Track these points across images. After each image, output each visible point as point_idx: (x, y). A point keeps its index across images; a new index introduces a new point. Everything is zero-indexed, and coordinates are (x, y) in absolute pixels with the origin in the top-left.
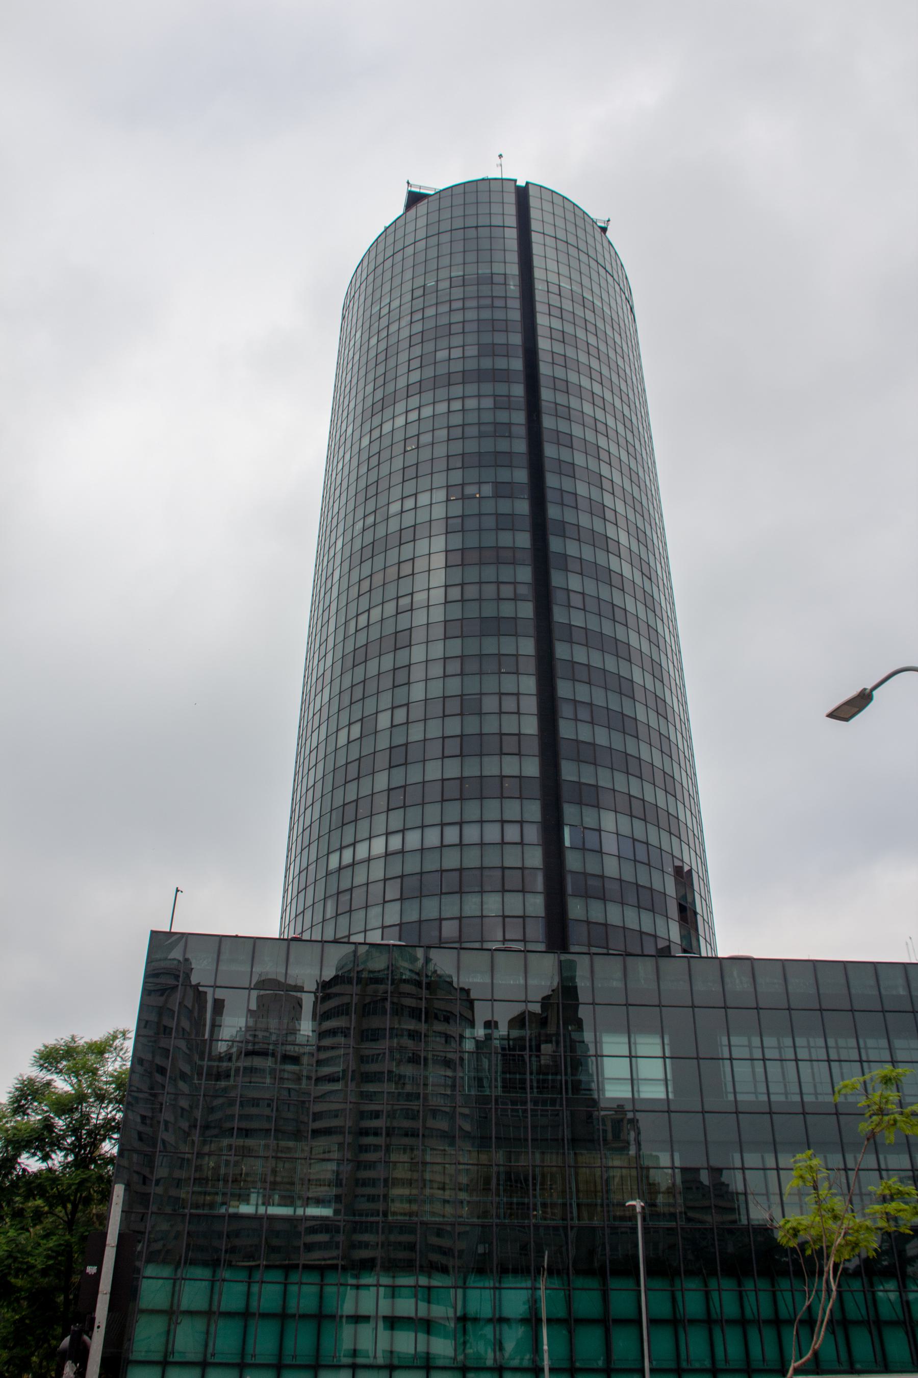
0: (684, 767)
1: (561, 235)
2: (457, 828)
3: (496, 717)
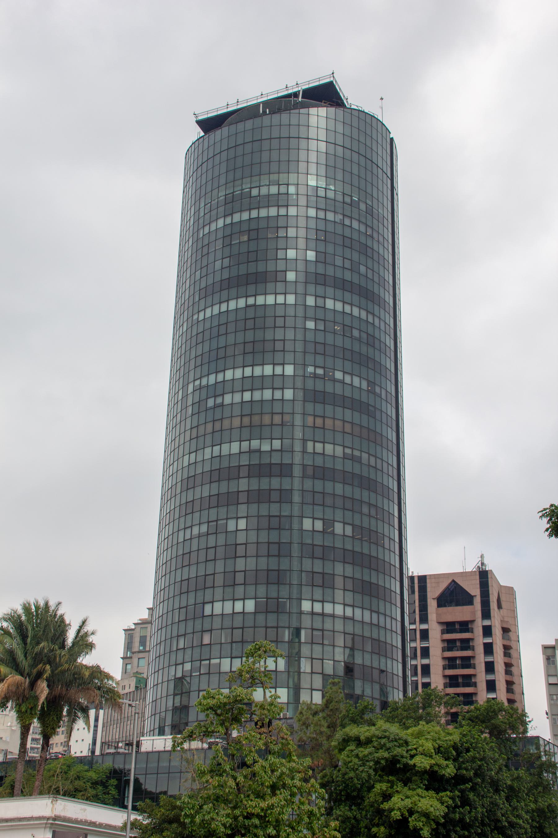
0: (385, 148)
1: (355, 148)
2: (249, 417)
3: (272, 330)
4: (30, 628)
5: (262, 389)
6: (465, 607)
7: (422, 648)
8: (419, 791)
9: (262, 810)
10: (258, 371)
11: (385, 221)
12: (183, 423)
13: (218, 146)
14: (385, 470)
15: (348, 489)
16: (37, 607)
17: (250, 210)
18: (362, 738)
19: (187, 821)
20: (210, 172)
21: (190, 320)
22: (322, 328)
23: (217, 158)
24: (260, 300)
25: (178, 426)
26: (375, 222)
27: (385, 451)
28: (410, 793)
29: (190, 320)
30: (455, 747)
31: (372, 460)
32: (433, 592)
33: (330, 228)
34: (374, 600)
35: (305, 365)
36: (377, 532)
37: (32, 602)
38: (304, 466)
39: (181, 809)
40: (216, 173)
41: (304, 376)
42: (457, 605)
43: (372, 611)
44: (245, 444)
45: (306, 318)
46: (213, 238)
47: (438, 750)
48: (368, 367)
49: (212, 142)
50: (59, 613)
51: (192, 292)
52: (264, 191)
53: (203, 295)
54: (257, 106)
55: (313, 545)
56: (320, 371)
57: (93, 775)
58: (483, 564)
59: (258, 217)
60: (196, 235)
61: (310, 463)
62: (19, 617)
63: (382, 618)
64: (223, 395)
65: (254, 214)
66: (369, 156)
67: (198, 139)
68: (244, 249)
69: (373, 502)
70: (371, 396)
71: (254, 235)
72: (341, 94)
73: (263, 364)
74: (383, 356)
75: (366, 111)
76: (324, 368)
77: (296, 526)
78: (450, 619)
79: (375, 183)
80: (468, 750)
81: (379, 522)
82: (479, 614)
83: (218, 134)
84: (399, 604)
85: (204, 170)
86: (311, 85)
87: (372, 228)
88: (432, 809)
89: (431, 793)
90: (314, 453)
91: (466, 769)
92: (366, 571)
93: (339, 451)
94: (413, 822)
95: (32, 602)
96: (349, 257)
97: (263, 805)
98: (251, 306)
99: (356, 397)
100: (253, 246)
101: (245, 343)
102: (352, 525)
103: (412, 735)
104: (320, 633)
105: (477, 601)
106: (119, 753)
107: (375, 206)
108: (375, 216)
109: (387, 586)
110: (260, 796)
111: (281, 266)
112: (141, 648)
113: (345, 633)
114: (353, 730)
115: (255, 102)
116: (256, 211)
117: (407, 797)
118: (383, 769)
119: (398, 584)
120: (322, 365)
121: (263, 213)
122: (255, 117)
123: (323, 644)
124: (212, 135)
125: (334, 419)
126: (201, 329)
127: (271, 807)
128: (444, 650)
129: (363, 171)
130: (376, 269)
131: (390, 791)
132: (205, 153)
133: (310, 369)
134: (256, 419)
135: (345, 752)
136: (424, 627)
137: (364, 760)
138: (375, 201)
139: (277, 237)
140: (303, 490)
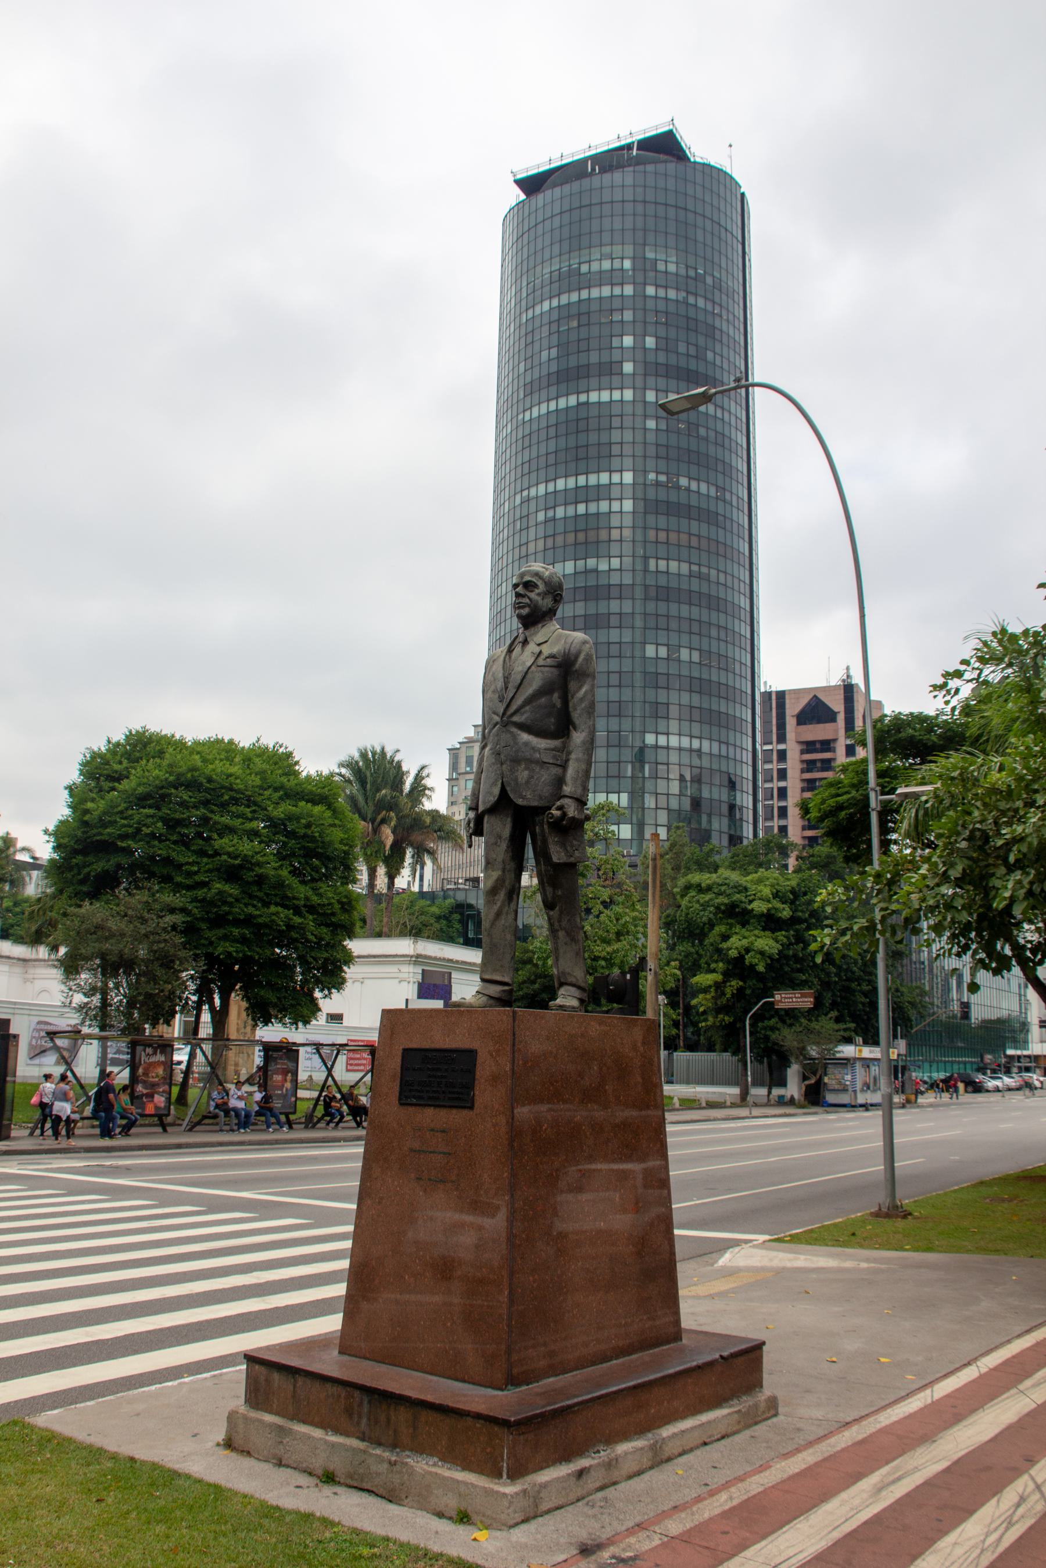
4: (368, 774)
5: (598, 500)
6: (828, 725)
7: (778, 770)
8: (756, 932)
9: (608, 953)
10: (593, 479)
11: (736, 296)
12: (511, 539)
13: (540, 212)
14: (736, 587)
15: (695, 610)
16: (374, 753)
17: (579, 289)
18: (703, 885)
19: (540, 963)
20: (532, 244)
21: (514, 421)
22: (664, 428)
23: (540, 227)
24: (594, 397)
25: (505, 543)
26: (724, 297)
27: (736, 566)
28: (747, 934)
29: (514, 421)
30: (793, 891)
31: (722, 576)
32: (792, 709)
33: (672, 308)
34: (724, 731)
35: (645, 472)
36: (727, 657)
37: (369, 748)
38: (646, 587)
39: (534, 953)
40: (539, 246)
41: (645, 484)
42: (819, 722)
43: (720, 742)
44: (580, 563)
45: (645, 417)
46: (537, 323)
47: (776, 895)
48: (716, 471)
49: (533, 208)
50: (396, 759)
51: (515, 388)
52: (595, 267)
53: (528, 391)
54: (584, 161)
55: (657, 674)
56: (663, 478)
57: (434, 909)
58: (848, 676)
59: (589, 299)
60: (517, 320)
61: (653, 583)
62: (357, 762)
63: (731, 749)
64: (554, 507)
65: (584, 294)
66: (715, 218)
67: (517, 205)
68: (573, 337)
69: (722, 623)
70: (720, 503)
71: (584, 320)
72: (683, 144)
73: (598, 472)
74: (734, 456)
75: (712, 163)
76: (667, 474)
77: (638, 653)
78: (810, 738)
79: (723, 251)
80: (805, 894)
81: (729, 646)
82: (842, 732)
83: (540, 199)
84: (750, 733)
85: (525, 242)
86: (648, 135)
87: (721, 306)
88: (767, 948)
89: (768, 933)
90: (657, 571)
91: (802, 911)
92: (714, 700)
93: (685, 568)
94: (748, 959)
95: (369, 748)
96: (694, 342)
97: (609, 949)
98: (583, 404)
99: (704, 505)
100: (584, 333)
101: (577, 447)
102: (700, 650)
103: (752, 881)
104: (665, 767)
105: (841, 718)
106: (459, 889)
107: (724, 278)
108: (724, 290)
109: (738, 714)
110: (606, 941)
111: (616, 356)
112: (468, 769)
113: (691, 767)
114: (696, 878)
115: (582, 156)
116: (587, 291)
117: (745, 938)
118: (723, 912)
119: (749, 712)
120: (665, 471)
121: (595, 293)
122: (583, 177)
123: (668, 778)
124: (533, 199)
125: (679, 532)
126: (527, 432)
127: (617, 951)
128: (803, 771)
129: (709, 236)
130: (725, 354)
131: (729, 932)
132: (526, 222)
133: (652, 476)
134: (592, 535)
135: (687, 898)
136: (782, 747)
137: (705, 906)
138: (724, 273)
139: (612, 321)
140: (645, 614)
